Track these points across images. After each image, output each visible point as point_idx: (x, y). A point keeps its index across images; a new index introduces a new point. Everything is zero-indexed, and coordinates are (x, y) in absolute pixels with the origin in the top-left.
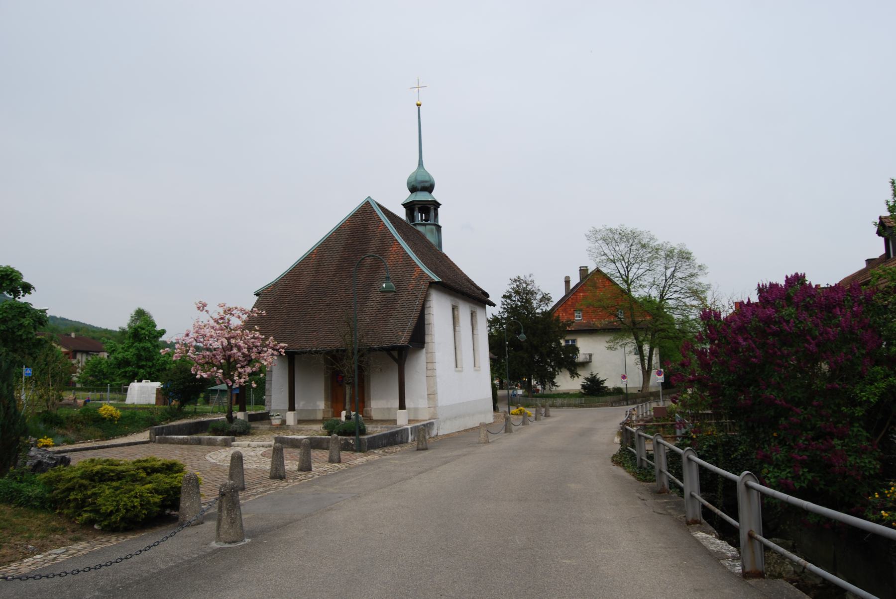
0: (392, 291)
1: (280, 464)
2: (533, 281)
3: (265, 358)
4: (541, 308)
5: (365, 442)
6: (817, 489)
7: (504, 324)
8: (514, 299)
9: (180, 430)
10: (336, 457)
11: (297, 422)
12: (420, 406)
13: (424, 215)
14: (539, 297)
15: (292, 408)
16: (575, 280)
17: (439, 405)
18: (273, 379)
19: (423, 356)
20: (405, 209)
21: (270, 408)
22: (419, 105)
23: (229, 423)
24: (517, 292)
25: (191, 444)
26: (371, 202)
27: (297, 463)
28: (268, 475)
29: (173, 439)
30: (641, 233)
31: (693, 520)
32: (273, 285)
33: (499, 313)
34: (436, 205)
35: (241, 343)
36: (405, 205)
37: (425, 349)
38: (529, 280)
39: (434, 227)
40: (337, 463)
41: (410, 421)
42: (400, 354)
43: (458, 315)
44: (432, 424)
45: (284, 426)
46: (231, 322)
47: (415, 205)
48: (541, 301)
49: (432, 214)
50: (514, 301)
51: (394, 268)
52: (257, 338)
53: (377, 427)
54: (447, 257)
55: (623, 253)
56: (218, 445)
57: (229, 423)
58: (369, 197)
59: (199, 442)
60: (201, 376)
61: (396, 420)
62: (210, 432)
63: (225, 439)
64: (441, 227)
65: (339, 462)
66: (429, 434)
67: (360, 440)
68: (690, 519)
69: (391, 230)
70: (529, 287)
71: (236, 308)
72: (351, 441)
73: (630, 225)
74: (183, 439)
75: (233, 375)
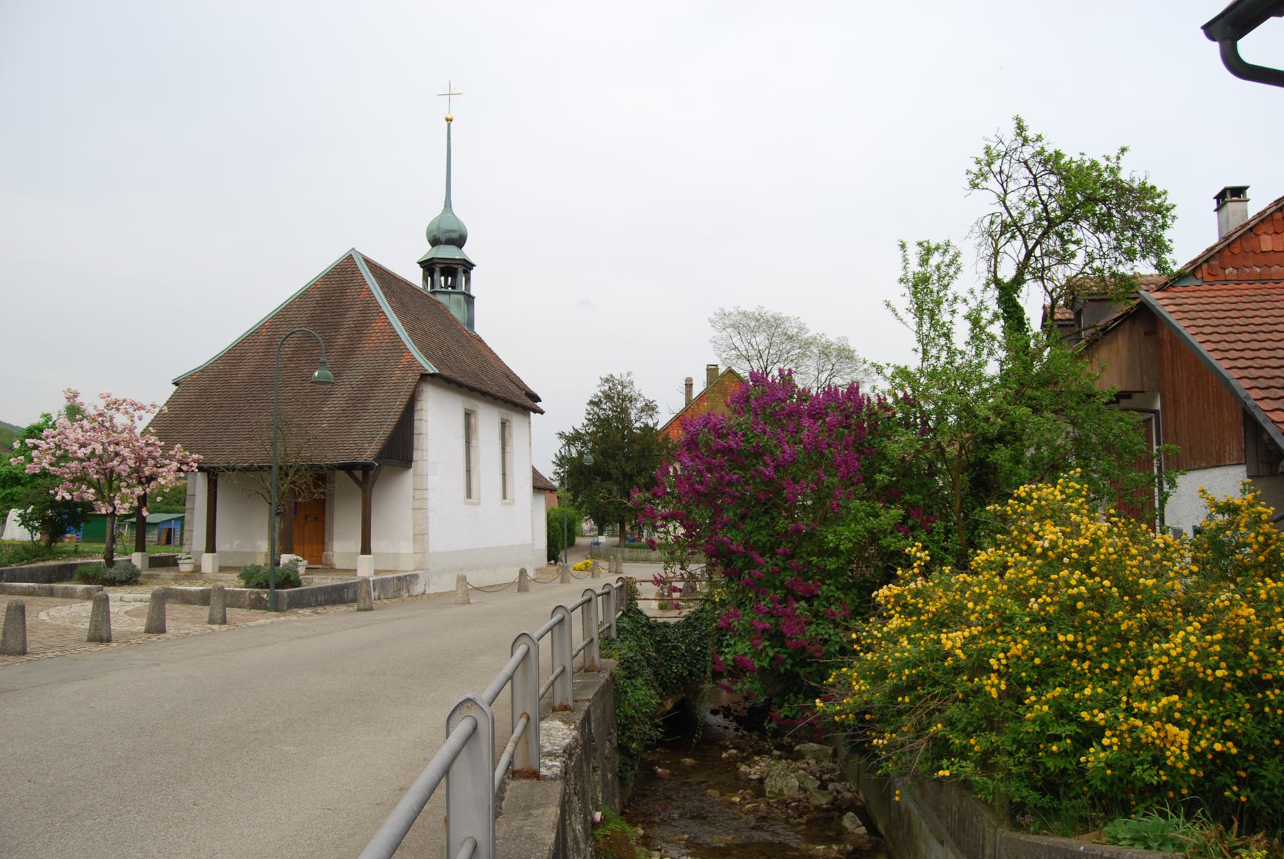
0: (329, 383)
1: (102, 621)
2: (631, 383)
3: (164, 474)
4: (642, 420)
5: (284, 598)
6: (782, 670)
7: (589, 441)
9: (32, 576)
10: (218, 616)
11: (147, 564)
12: (402, 552)
13: (450, 278)
14: (639, 405)
15: (211, 547)
18: (196, 506)
20: (422, 269)
21: (190, 548)
22: (449, 120)
23: (108, 566)
24: (608, 397)
25: (40, 596)
27: (145, 620)
28: (85, 638)
29: (14, 588)
30: (788, 319)
31: (561, 705)
32: (201, 371)
34: (468, 266)
35: (126, 452)
36: (422, 264)
37: (411, 471)
38: (626, 379)
39: (462, 297)
40: (221, 624)
41: (377, 572)
42: (366, 474)
43: (476, 423)
44: (416, 576)
45: (197, 574)
46: (114, 421)
47: (435, 263)
48: (642, 411)
50: (604, 410)
51: (375, 352)
52: (153, 444)
53: (326, 579)
55: (761, 348)
56: (78, 598)
57: (108, 566)
58: (353, 249)
59: (51, 593)
60: (63, 497)
61: (356, 570)
62: (79, 580)
63: (88, 589)
64: (473, 298)
65: (224, 622)
66: (408, 592)
67: (277, 595)
68: (557, 704)
70: (626, 391)
71: (124, 401)
72: (265, 596)
73: (772, 308)
74: (29, 587)
75: (114, 497)
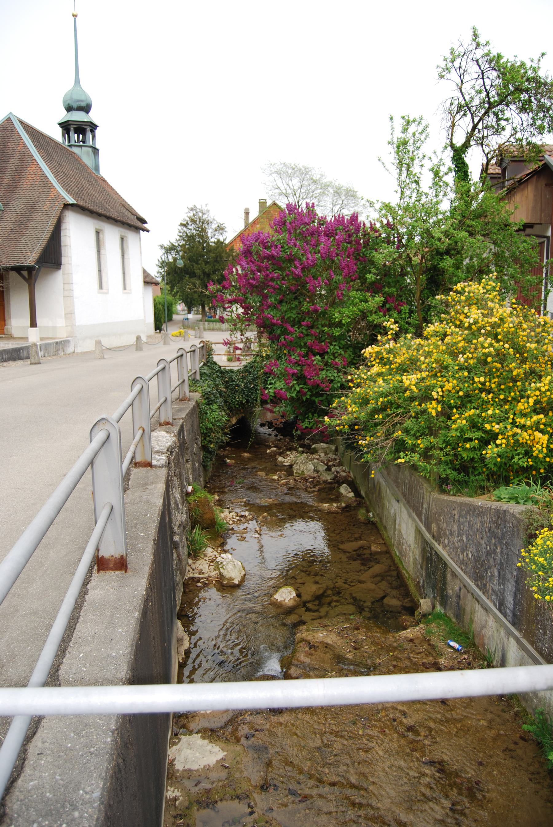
2: (208, 211)
6: (304, 399)
7: (180, 251)
8: (190, 227)
14: (214, 226)
16: (254, 214)
17: (77, 324)
19: (59, 277)
24: (193, 221)
26: (12, 119)
31: (165, 421)
33: (176, 240)
34: (93, 127)
36: (61, 124)
38: (204, 208)
39: (90, 150)
41: (42, 339)
42: (30, 273)
44: (68, 341)
47: (70, 125)
49: (89, 136)
54: (104, 180)
55: (296, 188)
69: (30, 149)
70: (205, 217)
